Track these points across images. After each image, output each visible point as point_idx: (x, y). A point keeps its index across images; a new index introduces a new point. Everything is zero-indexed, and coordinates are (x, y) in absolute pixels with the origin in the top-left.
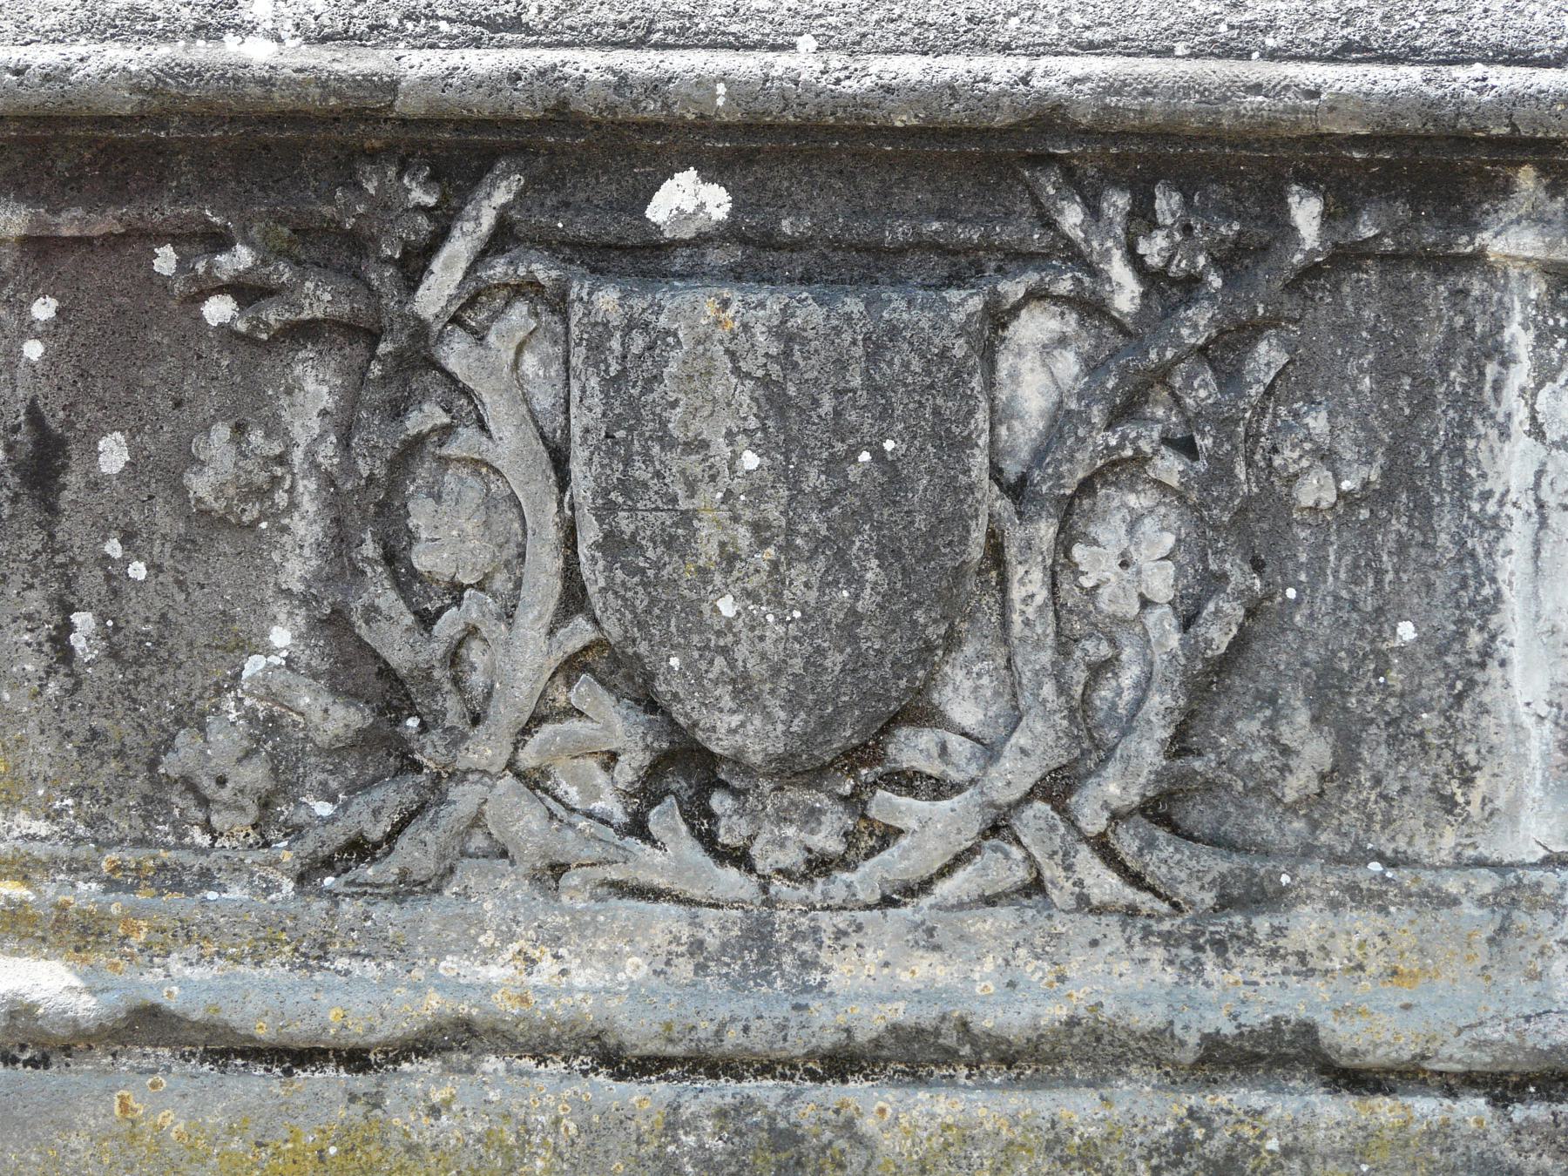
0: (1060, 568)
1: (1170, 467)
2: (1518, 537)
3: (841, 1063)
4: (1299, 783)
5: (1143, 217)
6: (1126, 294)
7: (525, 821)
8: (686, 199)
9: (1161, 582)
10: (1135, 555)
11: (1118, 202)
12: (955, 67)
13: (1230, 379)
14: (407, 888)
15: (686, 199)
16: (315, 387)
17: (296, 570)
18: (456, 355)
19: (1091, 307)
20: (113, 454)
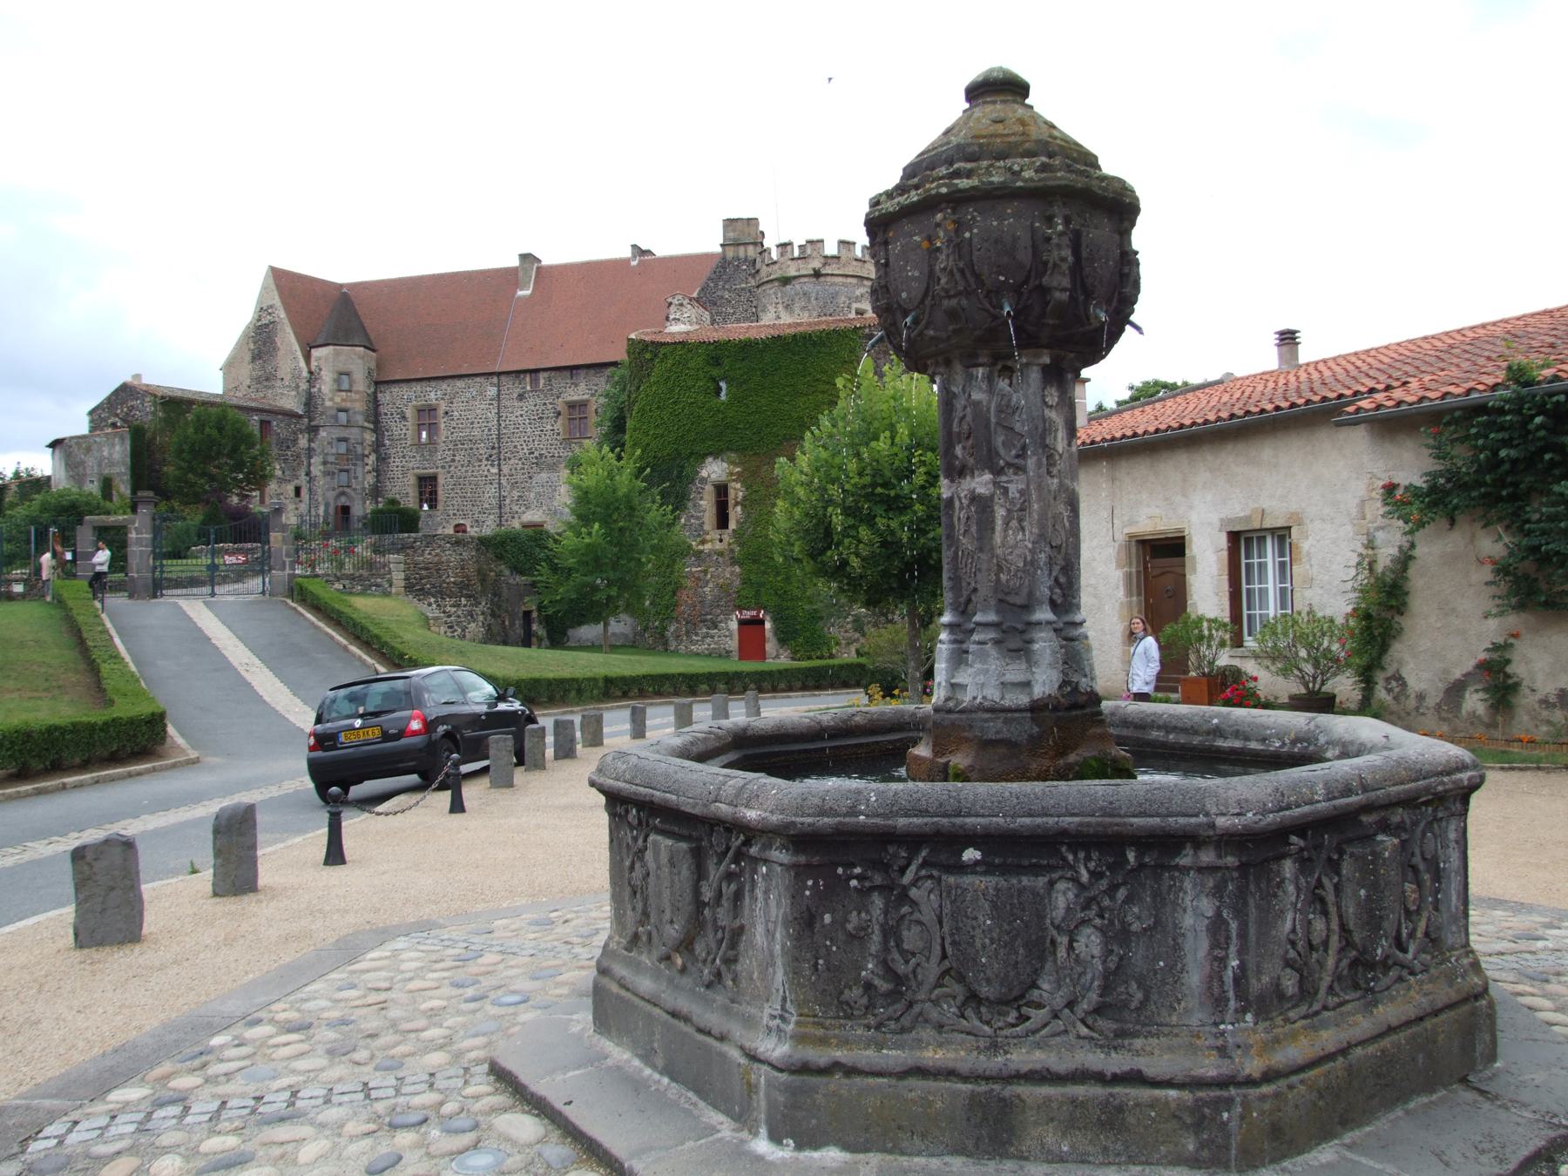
0: (1071, 948)
5: (1088, 858)
9: (1096, 951)
10: (1090, 943)
11: (1081, 855)
12: (1039, 820)
13: (1112, 898)
14: (903, 1030)
18: (913, 893)
19: (1075, 880)
20: (827, 918)
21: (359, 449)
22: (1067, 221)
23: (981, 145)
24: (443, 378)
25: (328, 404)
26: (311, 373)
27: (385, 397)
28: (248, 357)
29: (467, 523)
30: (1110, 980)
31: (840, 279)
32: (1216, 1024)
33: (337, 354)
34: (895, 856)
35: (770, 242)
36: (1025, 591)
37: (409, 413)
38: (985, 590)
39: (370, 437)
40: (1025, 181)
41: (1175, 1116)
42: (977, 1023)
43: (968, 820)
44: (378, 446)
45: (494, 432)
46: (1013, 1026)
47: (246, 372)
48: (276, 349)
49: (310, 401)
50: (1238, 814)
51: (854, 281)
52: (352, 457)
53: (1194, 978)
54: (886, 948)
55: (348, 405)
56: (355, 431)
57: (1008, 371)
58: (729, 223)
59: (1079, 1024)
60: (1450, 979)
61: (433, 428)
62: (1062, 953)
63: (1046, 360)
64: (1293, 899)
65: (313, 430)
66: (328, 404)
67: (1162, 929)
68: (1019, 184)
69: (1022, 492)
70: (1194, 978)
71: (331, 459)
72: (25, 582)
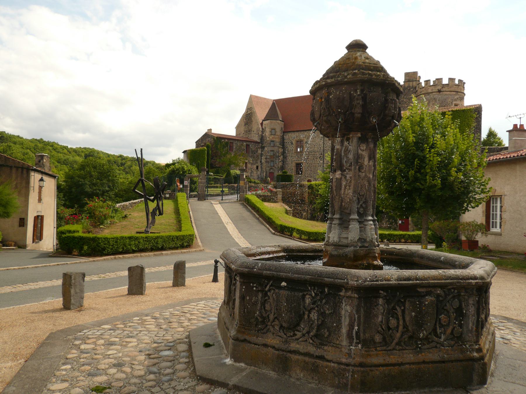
0: (309, 316)
1: (316, 308)
2: (343, 318)
3: (291, 352)
4: (326, 336)
5: (314, 289)
6: (313, 295)
7: (272, 329)
8: (284, 284)
9: (316, 318)
10: (314, 316)
11: (313, 288)
12: (300, 276)
14: (264, 333)
15: (284, 284)
16: (260, 295)
17: (258, 308)
19: (311, 295)
20: (248, 298)
21: (277, 154)
22: (362, 91)
23: (339, 68)
24: (305, 131)
25: (268, 139)
26: (263, 129)
27: (286, 137)
28: (243, 124)
29: (312, 179)
30: (319, 327)
31: (449, 93)
32: (349, 346)
33: (271, 123)
34: (264, 282)
35: (422, 81)
36: (349, 209)
37: (294, 142)
38: (337, 207)
39: (281, 150)
40: (348, 79)
41: (333, 372)
42: (283, 334)
43: (281, 274)
44: (283, 153)
45: (322, 149)
46: (291, 336)
47: (243, 129)
48: (252, 121)
49: (262, 138)
50: (356, 281)
51: (454, 93)
52: (274, 157)
53: (344, 330)
54: (261, 309)
55: (274, 139)
56: (276, 148)
57: (348, 139)
58: (407, 74)
59: (310, 339)
60: (462, 351)
61: (302, 147)
62: (306, 317)
63: (359, 135)
64: (382, 311)
65: (263, 148)
66: (268, 139)
67: (336, 313)
68: (346, 80)
69: (351, 177)
70: (344, 330)
71: (268, 157)
72: (170, 194)
